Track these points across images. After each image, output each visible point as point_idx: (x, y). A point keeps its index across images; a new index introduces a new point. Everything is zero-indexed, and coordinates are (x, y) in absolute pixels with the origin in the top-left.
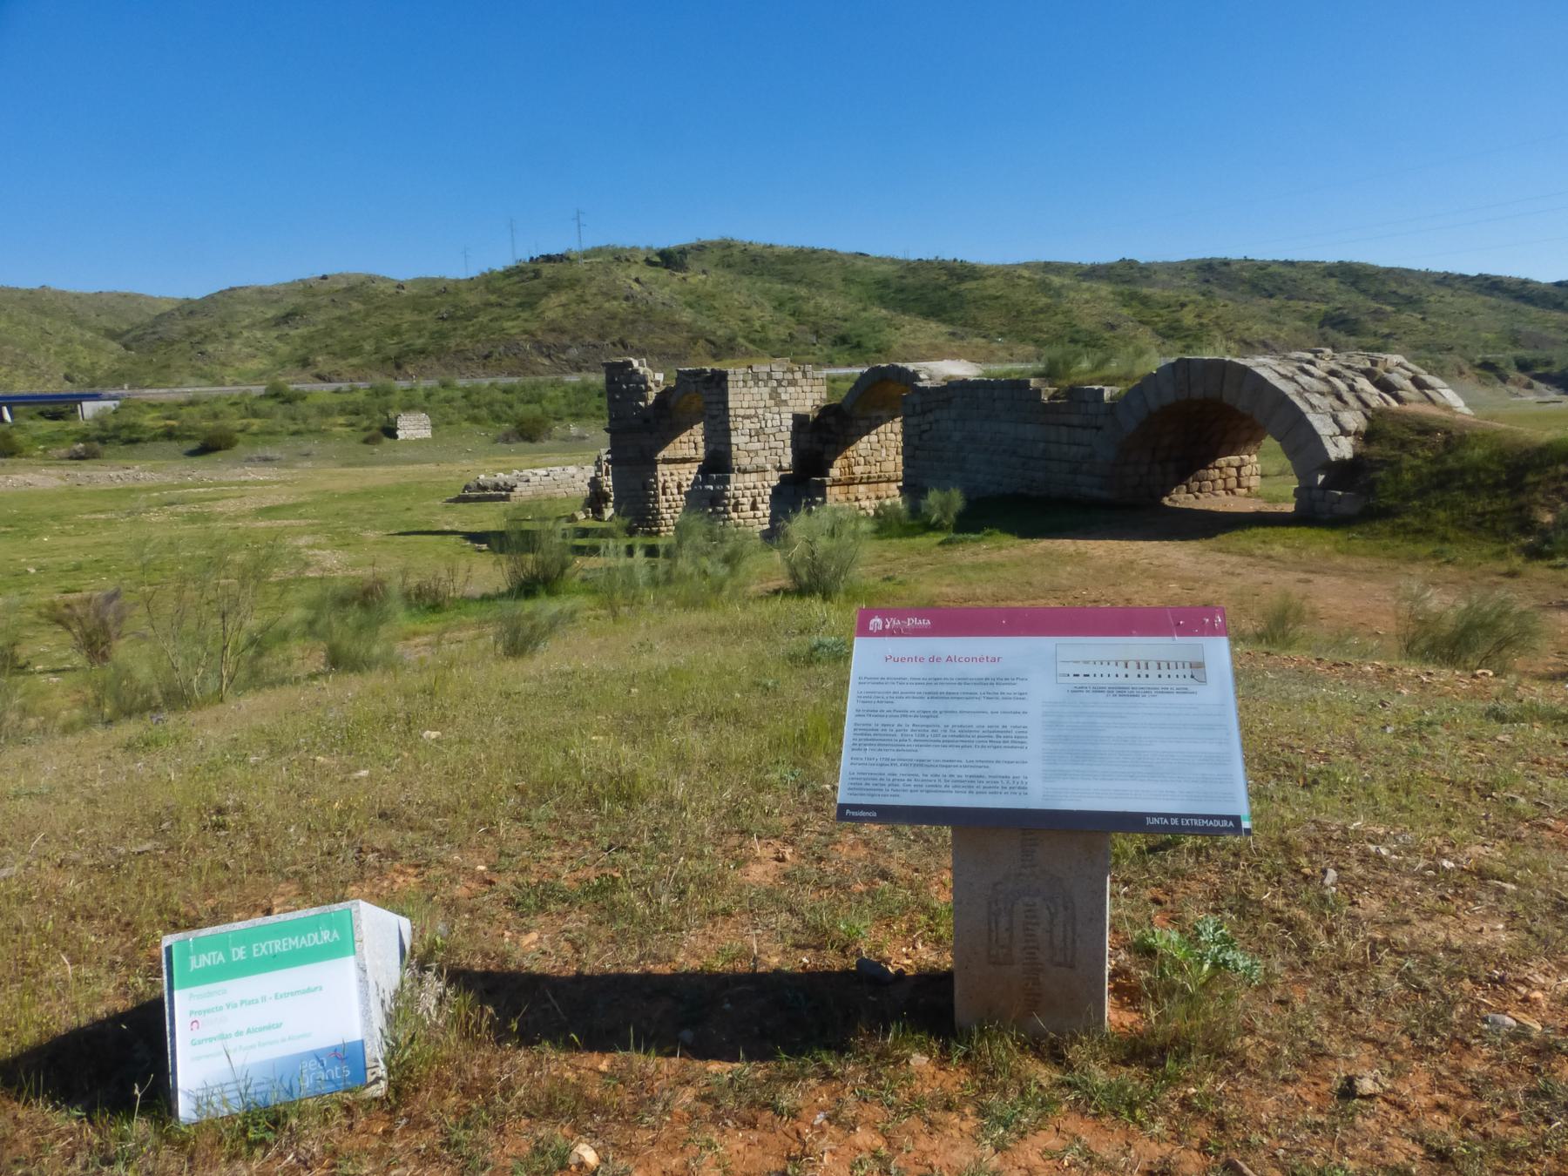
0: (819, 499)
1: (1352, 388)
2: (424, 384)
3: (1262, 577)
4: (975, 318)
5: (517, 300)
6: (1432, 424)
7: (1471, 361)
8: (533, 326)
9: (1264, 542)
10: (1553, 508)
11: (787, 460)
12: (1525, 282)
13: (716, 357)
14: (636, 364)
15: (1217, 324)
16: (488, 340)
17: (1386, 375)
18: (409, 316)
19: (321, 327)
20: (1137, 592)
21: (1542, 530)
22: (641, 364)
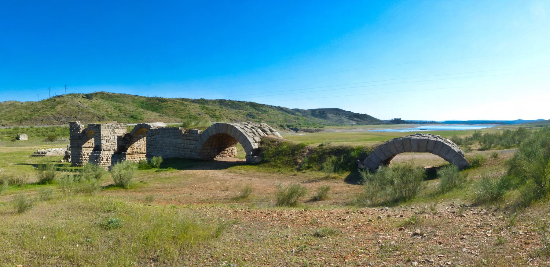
0: (124, 158)
1: (257, 131)
2: (26, 127)
3: (240, 179)
4: (165, 112)
5: (50, 107)
6: (275, 140)
7: (278, 125)
8: (54, 113)
9: (239, 169)
10: (301, 159)
11: (116, 148)
12: (287, 109)
13: (99, 121)
14: (77, 122)
15: (224, 115)
16: (42, 116)
17: (264, 128)
18: (24, 111)
19: (4, 113)
20: (209, 185)
21: (300, 164)
22: (79, 123)
